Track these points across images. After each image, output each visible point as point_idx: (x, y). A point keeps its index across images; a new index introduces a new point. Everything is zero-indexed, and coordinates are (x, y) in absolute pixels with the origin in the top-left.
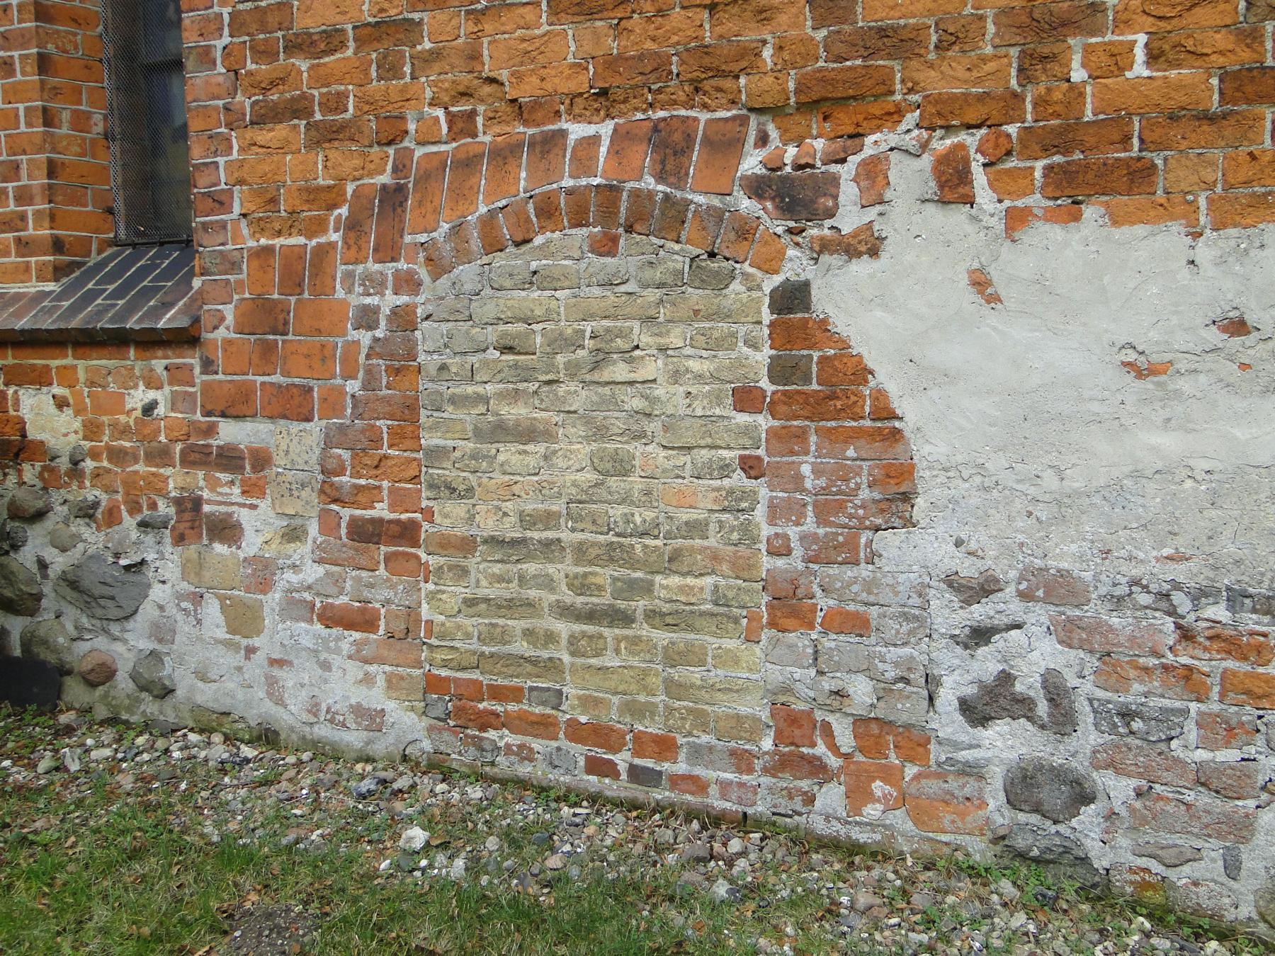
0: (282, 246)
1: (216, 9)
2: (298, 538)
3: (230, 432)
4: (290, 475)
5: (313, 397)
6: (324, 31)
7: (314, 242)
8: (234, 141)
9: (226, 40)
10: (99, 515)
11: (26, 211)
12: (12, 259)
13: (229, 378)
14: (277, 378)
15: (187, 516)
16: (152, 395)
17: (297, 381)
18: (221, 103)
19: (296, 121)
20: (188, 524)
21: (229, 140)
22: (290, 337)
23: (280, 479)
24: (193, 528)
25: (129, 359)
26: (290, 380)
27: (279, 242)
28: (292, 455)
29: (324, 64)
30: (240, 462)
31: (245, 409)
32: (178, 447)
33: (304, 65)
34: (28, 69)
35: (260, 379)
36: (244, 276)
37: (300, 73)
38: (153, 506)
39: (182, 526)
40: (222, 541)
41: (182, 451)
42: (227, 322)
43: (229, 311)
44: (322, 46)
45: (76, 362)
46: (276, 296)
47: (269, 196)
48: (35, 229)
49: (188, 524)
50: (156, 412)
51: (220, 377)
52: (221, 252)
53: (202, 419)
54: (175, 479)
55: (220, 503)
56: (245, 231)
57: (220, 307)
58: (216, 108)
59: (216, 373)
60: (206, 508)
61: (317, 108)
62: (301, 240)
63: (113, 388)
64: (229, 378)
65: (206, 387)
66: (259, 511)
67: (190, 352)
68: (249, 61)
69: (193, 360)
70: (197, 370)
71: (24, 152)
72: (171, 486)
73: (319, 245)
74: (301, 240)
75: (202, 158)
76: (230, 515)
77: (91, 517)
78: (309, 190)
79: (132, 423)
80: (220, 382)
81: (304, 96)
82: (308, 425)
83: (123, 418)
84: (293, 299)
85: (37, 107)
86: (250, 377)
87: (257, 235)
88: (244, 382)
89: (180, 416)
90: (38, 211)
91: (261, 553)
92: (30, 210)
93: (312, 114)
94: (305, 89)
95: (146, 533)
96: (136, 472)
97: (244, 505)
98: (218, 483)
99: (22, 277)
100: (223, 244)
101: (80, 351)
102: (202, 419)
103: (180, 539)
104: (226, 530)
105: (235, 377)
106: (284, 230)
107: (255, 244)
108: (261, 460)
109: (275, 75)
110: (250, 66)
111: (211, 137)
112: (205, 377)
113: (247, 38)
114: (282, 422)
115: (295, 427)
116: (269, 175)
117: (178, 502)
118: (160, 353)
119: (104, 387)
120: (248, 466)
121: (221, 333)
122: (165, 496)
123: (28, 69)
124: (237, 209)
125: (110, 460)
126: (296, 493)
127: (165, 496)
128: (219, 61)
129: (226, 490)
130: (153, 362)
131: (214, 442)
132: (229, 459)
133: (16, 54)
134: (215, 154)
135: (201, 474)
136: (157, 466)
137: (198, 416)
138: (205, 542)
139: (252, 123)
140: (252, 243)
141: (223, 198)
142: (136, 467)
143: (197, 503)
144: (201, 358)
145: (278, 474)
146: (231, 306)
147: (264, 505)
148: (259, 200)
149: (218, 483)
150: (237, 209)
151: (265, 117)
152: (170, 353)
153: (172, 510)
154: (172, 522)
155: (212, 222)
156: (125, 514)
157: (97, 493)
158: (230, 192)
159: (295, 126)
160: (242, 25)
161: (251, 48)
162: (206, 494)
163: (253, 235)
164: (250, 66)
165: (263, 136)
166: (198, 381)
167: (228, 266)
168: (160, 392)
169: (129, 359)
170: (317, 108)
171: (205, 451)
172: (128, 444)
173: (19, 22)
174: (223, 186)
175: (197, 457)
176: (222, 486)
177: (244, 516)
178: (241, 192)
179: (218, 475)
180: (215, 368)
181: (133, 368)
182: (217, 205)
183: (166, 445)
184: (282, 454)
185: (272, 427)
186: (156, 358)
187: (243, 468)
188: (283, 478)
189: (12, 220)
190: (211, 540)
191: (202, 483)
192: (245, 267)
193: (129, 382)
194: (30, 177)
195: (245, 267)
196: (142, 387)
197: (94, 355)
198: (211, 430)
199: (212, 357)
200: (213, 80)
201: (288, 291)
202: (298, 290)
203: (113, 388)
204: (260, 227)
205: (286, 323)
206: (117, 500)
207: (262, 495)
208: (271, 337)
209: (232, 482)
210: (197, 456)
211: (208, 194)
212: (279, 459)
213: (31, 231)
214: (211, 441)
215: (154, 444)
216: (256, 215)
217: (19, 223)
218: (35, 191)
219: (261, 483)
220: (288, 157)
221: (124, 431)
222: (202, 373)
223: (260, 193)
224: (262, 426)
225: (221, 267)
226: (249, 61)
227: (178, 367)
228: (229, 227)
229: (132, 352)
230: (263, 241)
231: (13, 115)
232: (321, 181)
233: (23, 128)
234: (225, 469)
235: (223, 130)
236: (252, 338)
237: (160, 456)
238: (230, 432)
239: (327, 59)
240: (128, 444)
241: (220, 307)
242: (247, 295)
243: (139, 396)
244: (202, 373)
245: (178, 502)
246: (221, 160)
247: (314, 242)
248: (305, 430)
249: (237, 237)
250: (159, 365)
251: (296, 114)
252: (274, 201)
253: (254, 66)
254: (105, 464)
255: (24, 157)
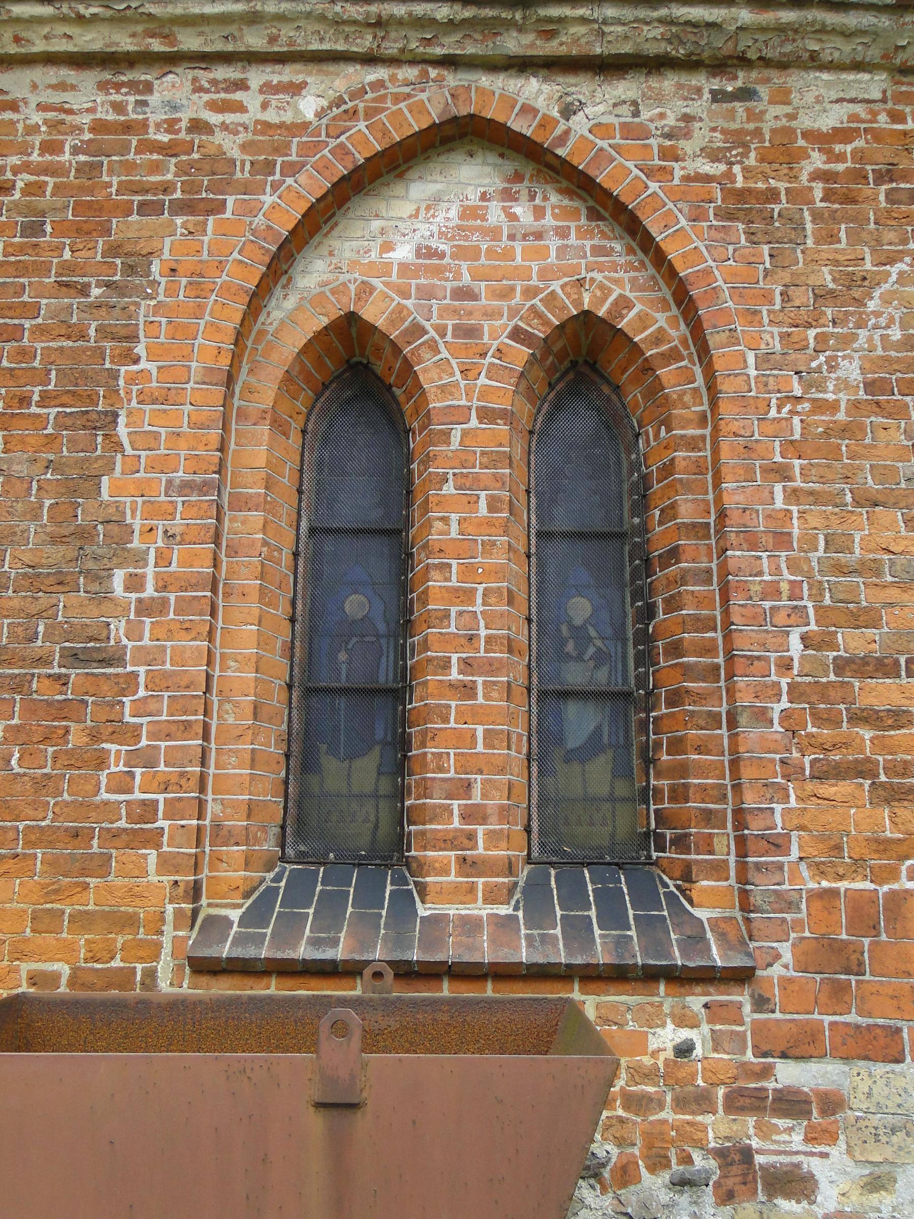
0: (847, 890)
1: (774, 678)
2: (883, 1187)
3: (789, 1074)
4: (875, 1120)
5: (902, 1038)
6: (889, 710)
7: (886, 888)
8: (791, 791)
9: (785, 704)
10: (606, 1174)
11: (476, 830)
12: (452, 878)
13: (788, 1017)
14: (852, 1018)
15: (736, 1169)
16: (685, 1034)
17: (880, 1021)
18: (778, 757)
19: (861, 780)
20: (738, 1179)
21: (786, 790)
22: (867, 977)
23: (862, 1124)
24: (745, 1184)
25: (658, 995)
26: (871, 1021)
27: (843, 885)
28: (876, 1097)
29: (891, 736)
30: (805, 1107)
31: (811, 1050)
32: (721, 1092)
33: (867, 734)
34: (495, 694)
35: (827, 1019)
36: (804, 914)
37: (863, 740)
38: (687, 1160)
39: (730, 1182)
40: (788, 1196)
41: (727, 1097)
42: (784, 960)
43: (786, 950)
44: (890, 722)
45: (583, 998)
46: (844, 936)
47: (832, 843)
48: (486, 849)
49: (738, 1179)
50: (695, 1053)
51: (778, 1015)
52: (775, 891)
53: (754, 1060)
54: (716, 1126)
55: (784, 1153)
56: (806, 874)
57: (774, 945)
58: (773, 761)
59: (773, 1012)
60: (759, 1159)
61: (881, 771)
62: (868, 885)
63: (631, 1026)
64: (788, 1017)
65: (758, 1029)
66: (832, 1159)
67: (737, 989)
68: (810, 725)
69: (743, 998)
70: (747, 1008)
71: (480, 772)
72: (711, 1135)
73: (893, 892)
74: (868, 885)
75: (755, 803)
76: (798, 1166)
77: (597, 1176)
78: (878, 841)
79: (661, 1066)
80: (778, 1021)
81: (868, 760)
82: (898, 1067)
83: (647, 1060)
84: (866, 941)
85: (502, 731)
86: (816, 1016)
87: (818, 878)
88: (808, 1022)
89: (726, 1057)
90: (494, 831)
91: (840, 1208)
92: (480, 830)
93: (878, 776)
94: (869, 754)
95: (682, 1192)
96: (664, 1122)
97: (812, 1154)
98: (776, 1130)
99: (461, 898)
100: (778, 884)
101: (592, 986)
102: (754, 1060)
103: (727, 1197)
104: (793, 1183)
105: (796, 1016)
106: (848, 875)
107: (817, 886)
108: (831, 1103)
109: (838, 739)
110: (811, 729)
111: (765, 785)
112: (757, 1016)
113: (807, 706)
114: (862, 1063)
115: (880, 1069)
116: (833, 825)
117: (721, 1154)
118: (698, 989)
119: (620, 1025)
120: (818, 1112)
121: (776, 971)
122: (701, 1146)
123: (495, 694)
124: (795, 853)
125: (626, 1107)
126: (884, 1139)
127: (701, 1146)
128: (776, 721)
129: (785, 1137)
130: (688, 999)
131: (771, 1085)
132: (791, 1103)
133: (480, 680)
134: (771, 801)
135: (751, 1121)
136: (693, 1113)
137: (749, 1055)
138: (761, 1197)
139: (813, 777)
140: (812, 885)
141: (779, 841)
142: (662, 1115)
143: (747, 1154)
144: (752, 996)
145: (858, 1119)
146: (789, 944)
147: (837, 1152)
148: (821, 846)
149: (776, 1130)
150: (795, 853)
151: (825, 773)
152: (711, 990)
153: (713, 1164)
154: (715, 1178)
155: (766, 863)
156: (643, 1171)
157: (608, 1147)
158: (788, 836)
159: (861, 785)
160: (801, 694)
161: (811, 714)
162: (755, 1143)
163: (812, 878)
164: (811, 729)
165: (828, 789)
166: (748, 1020)
167: (783, 905)
168: (695, 1031)
169: (658, 995)
170: (881, 771)
171: (759, 1096)
172: (651, 1089)
173: (486, 651)
174: (779, 830)
175: (744, 1101)
176: (780, 1133)
177: (814, 1165)
178: (800, 837)
179: (774, 1121)
180: (771, 1006)
181: (661, 1005)
182: (772, 848)
183: (704, 1089)
184: (863, 1097)
185: (846, 1068)
186: (693, 994)
187: (810, 1113)
188: (867, 1123)
189: (455, 838)
190: (771, 1196)
191: (752, 1131)
192: (804, 906)
193: (654, 1020)
194: (484, 796)
195: (804, 906)
196: (670, 1026)
197: (612, 990)
198: (766, 1072)
199: (767, 995)
200: (770, 737)
201: (863, 933)
202: (874, 933)
203: (631, 1026)
204: (820, 870)
205: (861, 964)
206: (633, 1155)
207: (833, 1139)
208: (843, 977)
209: (790, 1130)
210: (748, 1101)
211: (762, 837)
212: (859, 1103)
213: (481, 850)
214: (765, 1084)
215: (691, 1088)
216: (817, 859)
217: (466, 841)
218: (489, 811)
219: (832, 1128)
220: (853, 811)
221: (649, 1075)
222: (754, 1011)
223: (822, 839)
224: (830, 1067)
225: (776, 906)
226: (810, 725)
227: (722, 1005)
228: (786, 868)
229: (662, 988)
230: (825, 884)
231: (470, 735)
232: (888, 834)
233: (480, 748)
234: (785, 1114)
235: (779, 780)
236: (818, 977)
237: (702, 1101)
238: (789, 1074)
239: (892, 733)
240: (651, 1089)
241: (774, 945)
242: (807, 934)
243: (667, 1037)
244: (754, 1011)
245: (721, 1154)
246: (778, 808)
247: (886, 888)
248: (893, 1072)
249: (795, 876)
250: (696, 1002)
251: (861, 774)
252: (838, 848)
253: (815, 730)
254: (620, 1112)
255: (479, 777)
